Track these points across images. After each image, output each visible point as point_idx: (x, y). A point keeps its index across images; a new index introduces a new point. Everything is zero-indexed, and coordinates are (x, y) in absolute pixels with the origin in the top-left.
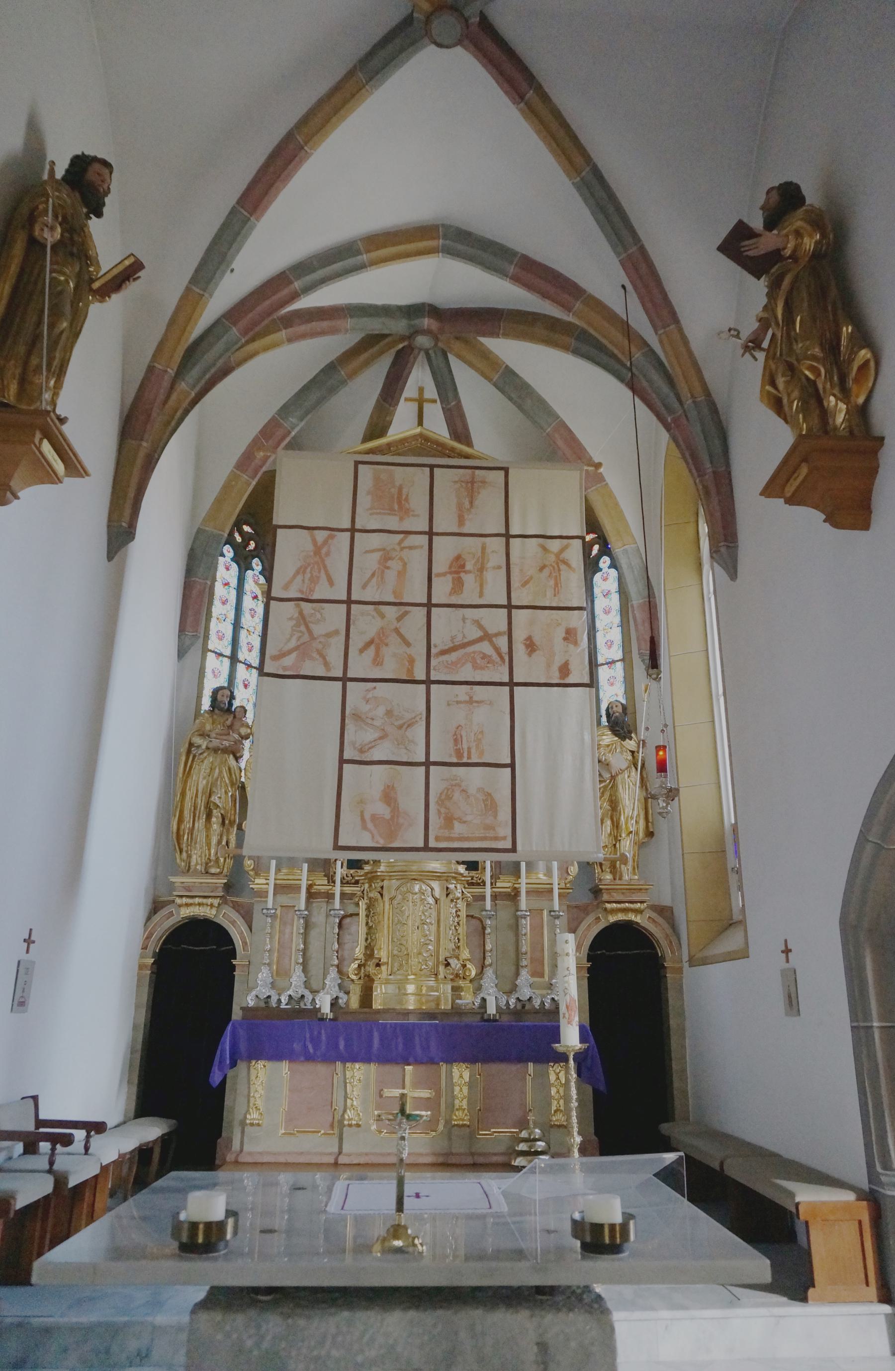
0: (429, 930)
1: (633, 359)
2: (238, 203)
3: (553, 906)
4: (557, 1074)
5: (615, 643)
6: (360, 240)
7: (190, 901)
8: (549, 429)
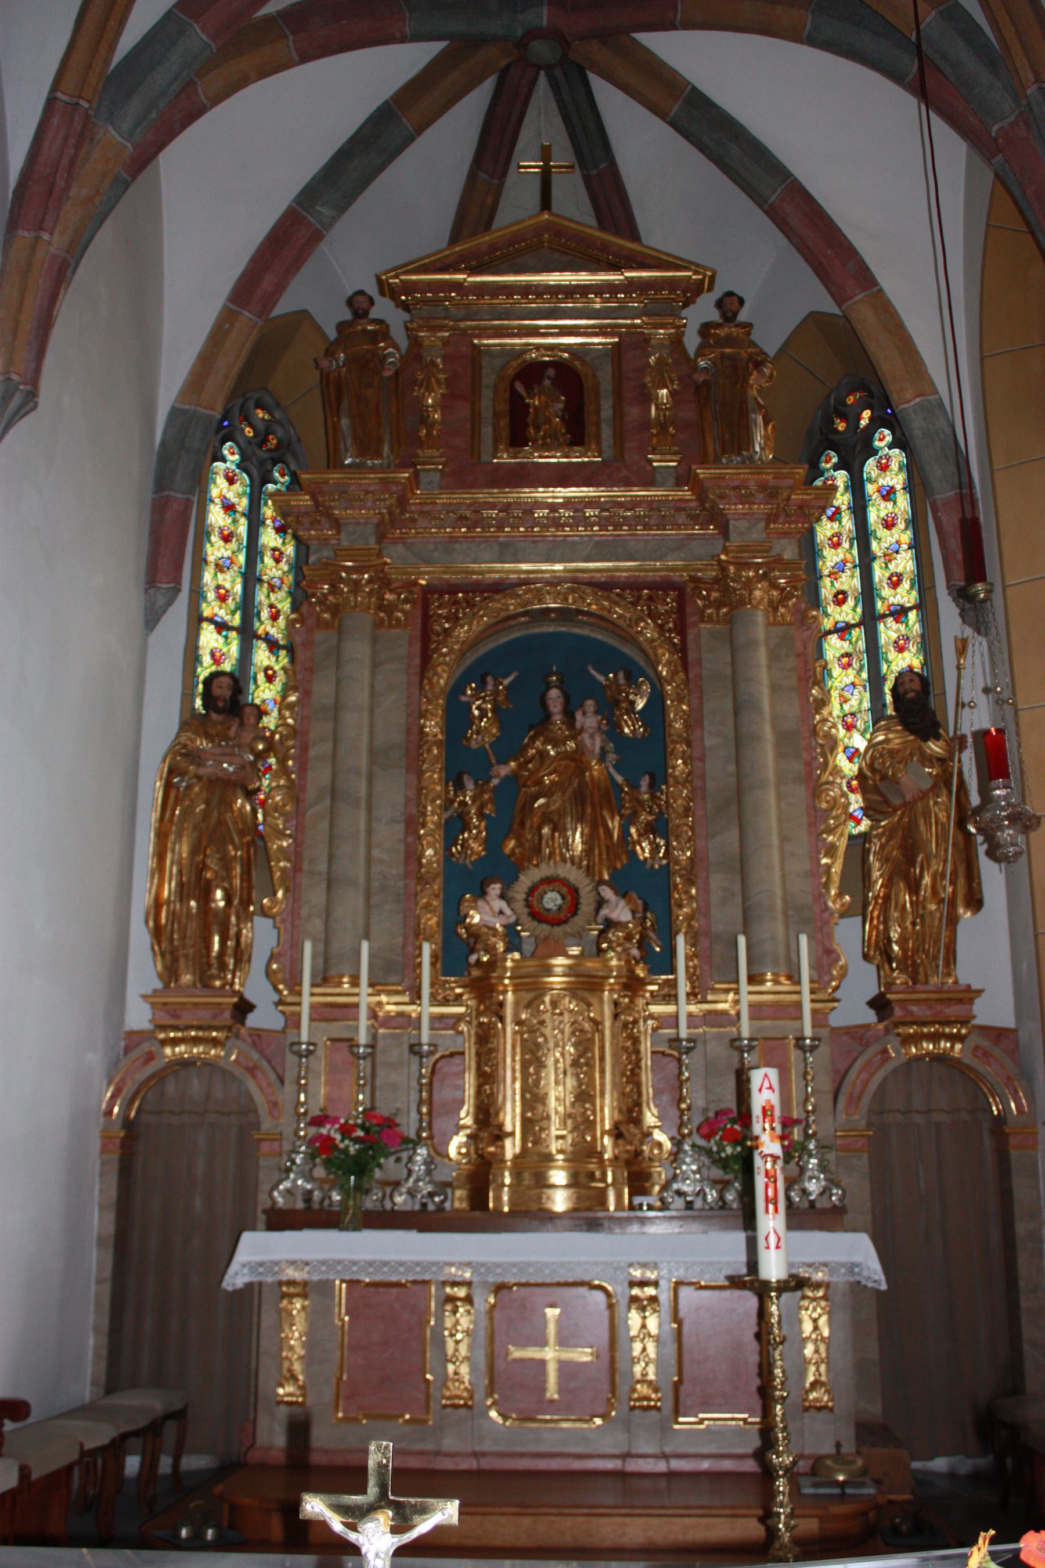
1: (922, 27)
3: (802, 1030)
4: (815, 1321)
5: (905, 576)
8: (774, 198)
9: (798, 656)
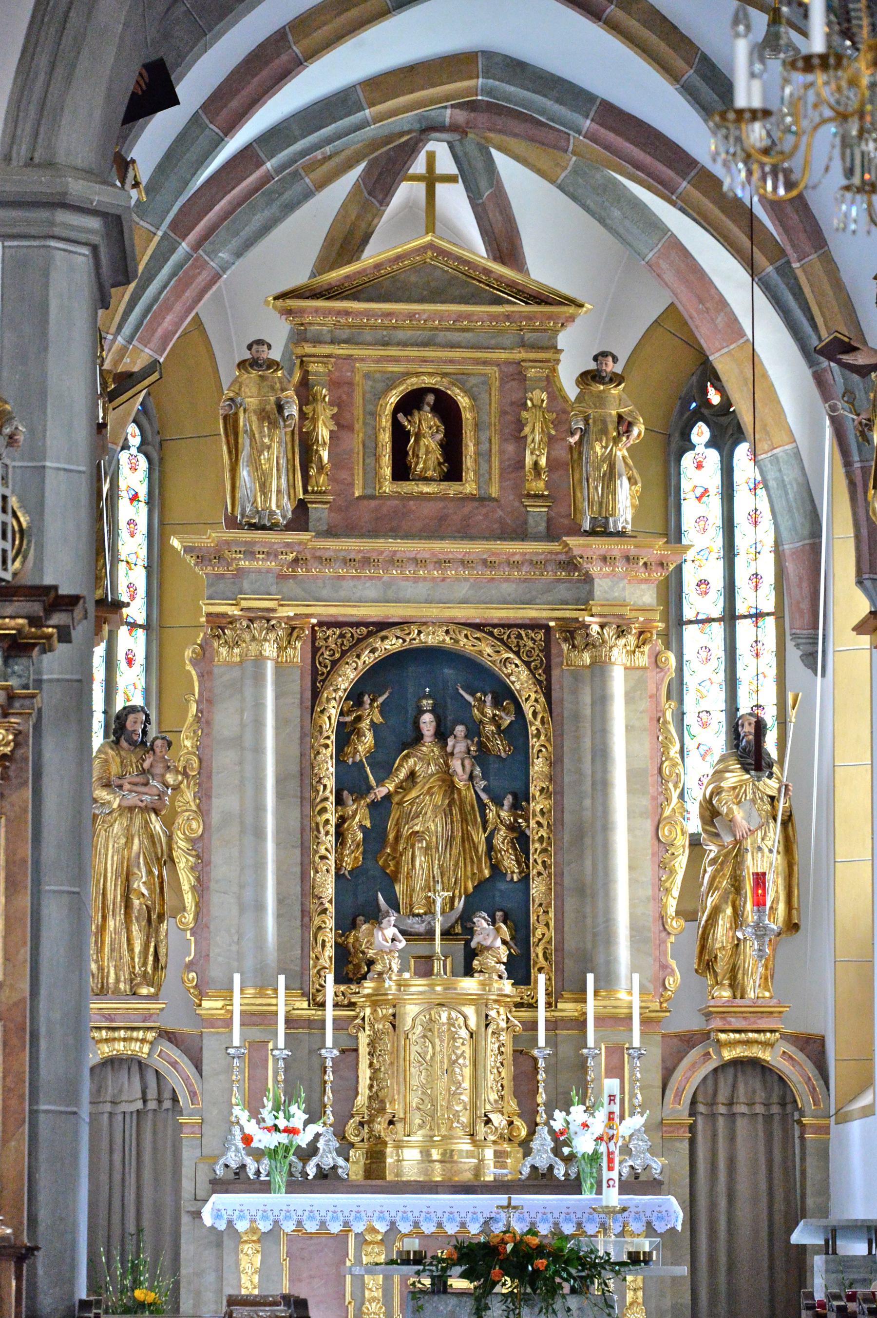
0: (462, 1075)
2: (205, 107)
6: (360, 84)
7: (111, 1034)
8: (651, 255)
9: (651, 697)
